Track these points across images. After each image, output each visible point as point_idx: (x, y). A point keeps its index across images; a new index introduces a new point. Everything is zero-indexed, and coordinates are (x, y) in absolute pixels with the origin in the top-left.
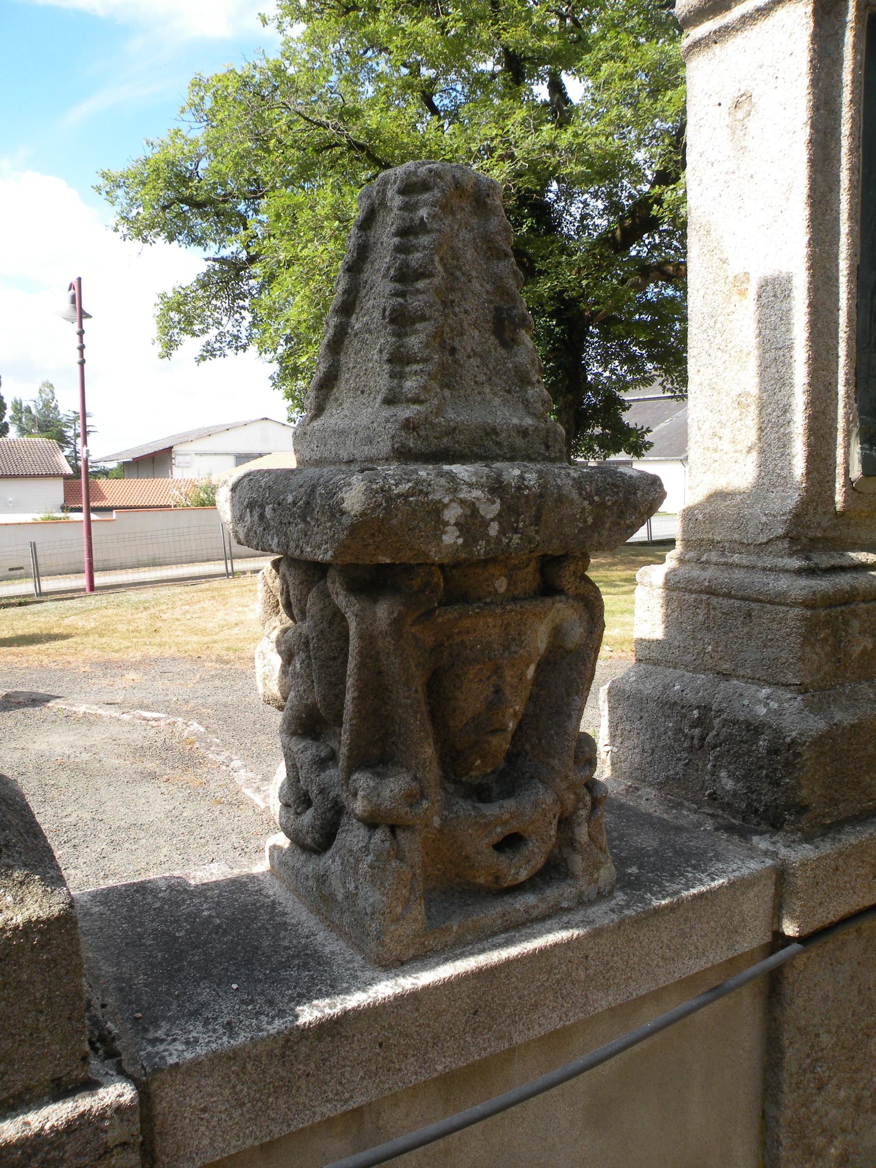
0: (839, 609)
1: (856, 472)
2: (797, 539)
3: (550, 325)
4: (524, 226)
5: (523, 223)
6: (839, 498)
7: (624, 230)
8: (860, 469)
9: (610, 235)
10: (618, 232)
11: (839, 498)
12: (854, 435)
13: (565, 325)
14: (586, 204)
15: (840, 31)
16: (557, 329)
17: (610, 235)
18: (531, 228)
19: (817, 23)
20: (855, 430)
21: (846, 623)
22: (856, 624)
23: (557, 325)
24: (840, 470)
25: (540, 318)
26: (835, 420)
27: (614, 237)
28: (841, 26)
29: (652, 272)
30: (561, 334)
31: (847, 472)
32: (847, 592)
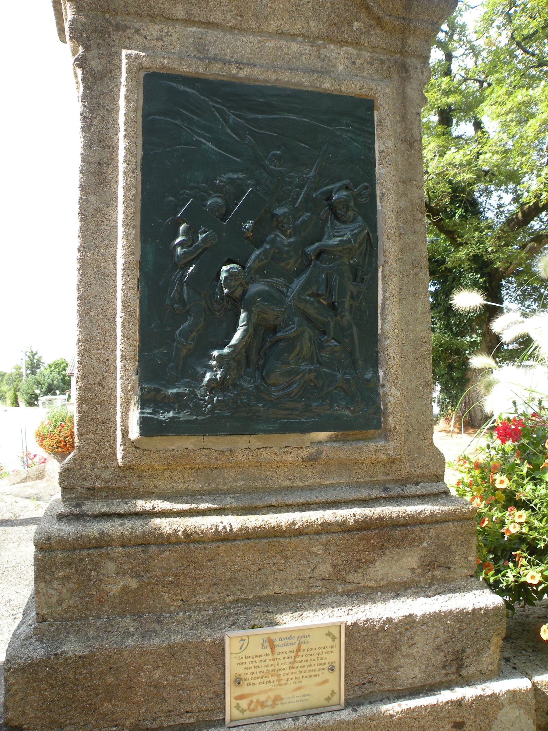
0: (85, 552)
1: (134, 433)
2: (72, 489)
3: (476, 278)
4: (457, 215)
5: (456, 213)
6: (119, 455)
7: (523, 213)
8: (138, 430)
9: (514, 216)
10: (520, 215)
11: (119, 455)
12: (133, 401)
13: (486, 277)
14: (500, 198)
15: (115, 89)
16: (481, 280)
17: (514, 216)
18: (461, 216)
19: (87, 87)
20: (135, 398)
21: (96, 565)
22: (111, 566)
23: (480, 278)
24: (119, 433)
25: (469, 274)
26: (114, 390)
27: (517, 218)
28: (116, 86)
29: (544, 239)
30: (483, 283)
31: (125, 433)
32: (94, 538)
